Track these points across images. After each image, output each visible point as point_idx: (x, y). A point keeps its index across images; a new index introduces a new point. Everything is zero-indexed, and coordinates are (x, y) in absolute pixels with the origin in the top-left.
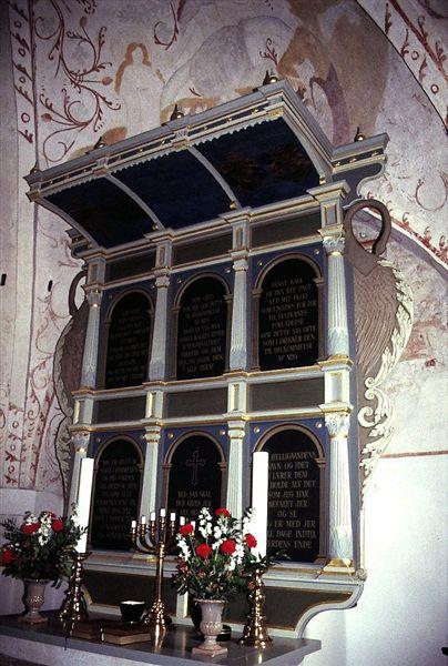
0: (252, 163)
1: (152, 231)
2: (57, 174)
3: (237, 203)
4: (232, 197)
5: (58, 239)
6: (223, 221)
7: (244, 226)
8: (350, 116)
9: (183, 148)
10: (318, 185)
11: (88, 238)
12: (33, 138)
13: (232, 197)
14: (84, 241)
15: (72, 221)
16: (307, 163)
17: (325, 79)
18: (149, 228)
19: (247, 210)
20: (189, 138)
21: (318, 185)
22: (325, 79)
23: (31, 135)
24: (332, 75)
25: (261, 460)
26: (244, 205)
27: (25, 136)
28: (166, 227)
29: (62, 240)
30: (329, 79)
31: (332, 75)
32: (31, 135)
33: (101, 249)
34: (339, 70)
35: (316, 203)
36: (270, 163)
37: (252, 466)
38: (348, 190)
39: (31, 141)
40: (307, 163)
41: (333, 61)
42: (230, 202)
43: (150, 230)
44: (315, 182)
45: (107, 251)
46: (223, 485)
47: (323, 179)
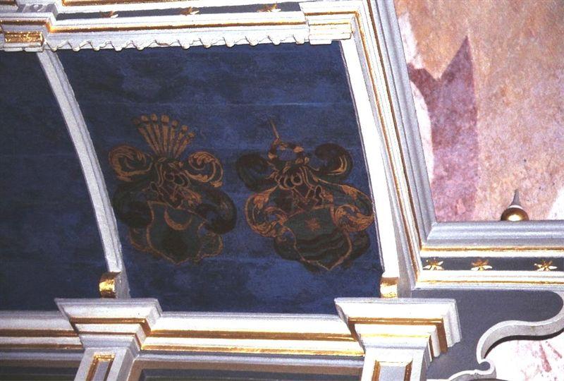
0: (207, 169)
3: (123, 282)
4: (114, 262)
6: (64, 325)
7: (119, 354)
8: (480, 183)
9: (29, 46)
10: (376, 293)
13: (114, 262)
17: (437, 75)
18: (84, 280)
19: (145, 309)
20: (55, 25)
21: (376, 293)
22: (437, 75)
24: (460, 69)
25: (20, 49)
26: (139, 288)
30: (450, 76)
31: (460, 69)
34: (482, 64)
35: (352, 348)
36: (256, 186)
38: (454, 335)
41: (469, 34)
42: (104, 273)
43: (92, 293)
44: (367, 280)
46: (304, 372)
47: (391, 282)
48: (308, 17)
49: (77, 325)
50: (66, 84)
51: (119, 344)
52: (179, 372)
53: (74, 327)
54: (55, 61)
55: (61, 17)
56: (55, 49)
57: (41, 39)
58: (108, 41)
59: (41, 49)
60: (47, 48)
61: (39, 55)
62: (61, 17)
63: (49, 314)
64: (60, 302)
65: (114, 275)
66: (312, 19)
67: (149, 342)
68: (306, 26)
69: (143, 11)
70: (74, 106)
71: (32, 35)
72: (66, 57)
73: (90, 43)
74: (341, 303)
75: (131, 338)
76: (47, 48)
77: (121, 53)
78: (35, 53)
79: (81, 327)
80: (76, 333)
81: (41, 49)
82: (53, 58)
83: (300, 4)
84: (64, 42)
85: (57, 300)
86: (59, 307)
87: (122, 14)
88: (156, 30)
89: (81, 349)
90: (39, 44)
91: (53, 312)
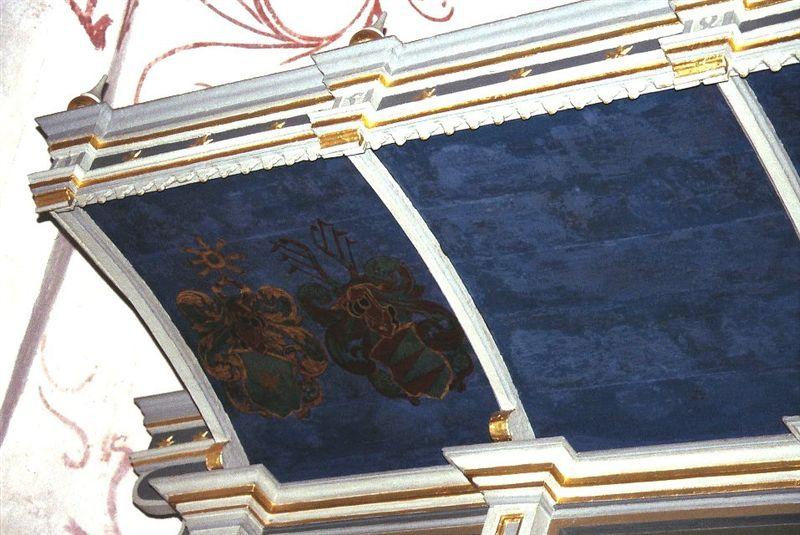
1: (485, 438)
2: (161, 125)
5: (96, 442)
11: (220, 426)
12: (112, 34)
13: (506, 395)
14: (203, 444)
15: (188, 364)
16: (223, 372)
18: (475, 422)
23: (106, 21)
27: (85, 21)
28: (543, 430)
29: (110, 447)
32: (106, 21)
33: (259, 476)
37: (166, 394)
39: (98, 40)
40: (223, 372)
43: (480, 436)
45: (277, 493)
48: (665, 61)
49: (475, 480)
50: (763, 119)
51: (525, 500)
52: (696, 523)
53: (470, 480)
54: (744, 90)
55: (746, 27)
56: (745, 74)
57: (724, 64)
58: (173, 179)
59: (725, 77)
60: (733, 73)
61: (356, 161)
62: (746, 27)
63: (776, 439)
64: (449, 453)
65: (506, 415)
66: (675, 58)
67: (269, 518)
68: (670, 68)
69: (450, 84)
70: (777, 148)
71: (711, 60)
72: (389, 155)
73: (795, 56)
74: (448, 452)
75: (242, 512)
76: (733, 73)
77: (776, 75)
78: (715, 84)
79: (479, 481)
80: (476, 489)
81: (725, 77)
82: (742, 86)
83: (660, 41)
84: (91, 196)
85: (786, 419)
86: (792, 429)
87: (217, 137)
88: (760, 49)
89: (482, 509)
90: (723, 70)
91: (783, 436)
